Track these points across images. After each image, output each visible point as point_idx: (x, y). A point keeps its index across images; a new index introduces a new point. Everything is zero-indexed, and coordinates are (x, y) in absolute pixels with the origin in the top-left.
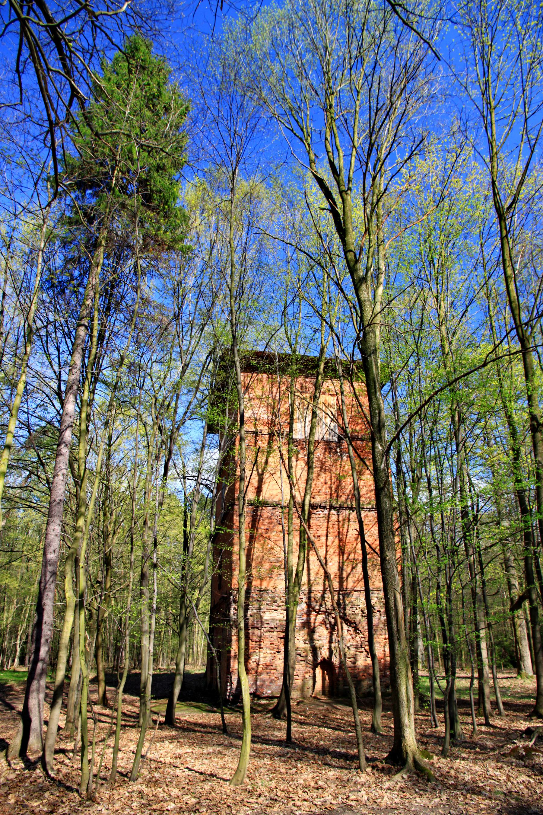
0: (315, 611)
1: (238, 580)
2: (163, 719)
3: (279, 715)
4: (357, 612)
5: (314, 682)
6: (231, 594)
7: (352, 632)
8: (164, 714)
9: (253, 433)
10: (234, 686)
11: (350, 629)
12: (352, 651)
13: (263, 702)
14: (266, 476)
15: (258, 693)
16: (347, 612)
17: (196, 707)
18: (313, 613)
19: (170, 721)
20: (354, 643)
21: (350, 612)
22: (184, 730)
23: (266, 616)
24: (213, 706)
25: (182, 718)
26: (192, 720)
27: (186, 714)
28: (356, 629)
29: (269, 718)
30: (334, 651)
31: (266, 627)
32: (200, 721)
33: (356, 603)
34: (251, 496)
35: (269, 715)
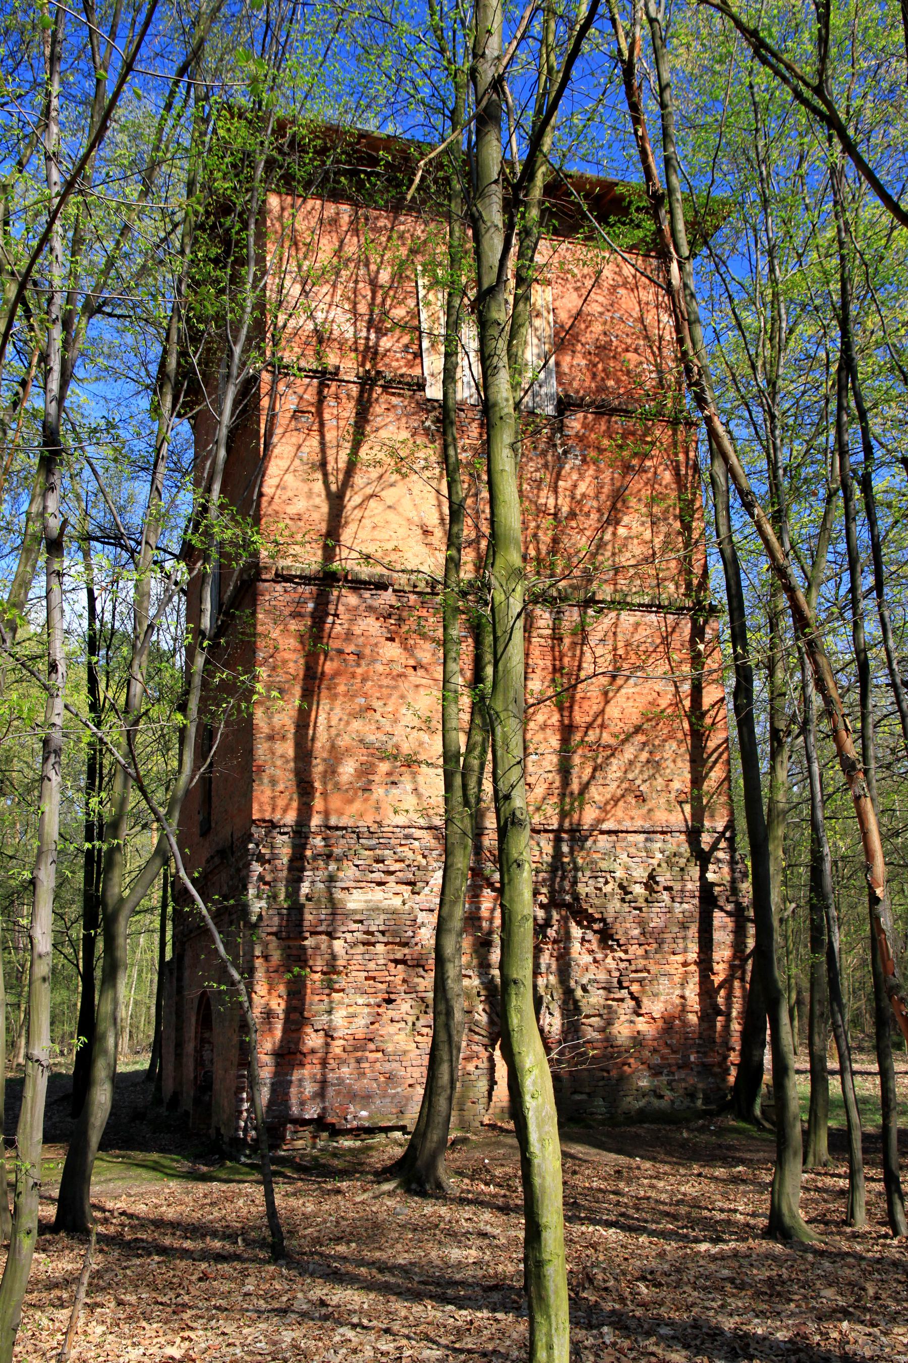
0: (491, 885)
1: (273, 799)
2: (50, 1212)
3: (421, 1184)
4: (608, 889)
5: (492, 1083)
6: (249, 837)
7: (595, 946)
8: (56, 1193)
9: (314, 374)
10: (264, 1095)
11: (590, 935)
12: (596, 998)
13: (347, 1143)
14: (352, 500)
15: (330, 1119)
16: (582, 889)
17: (155, 1167)
18: (488, 893)
19: (71, 1218)
20: (602, 976)
21: (590, 890)
22: (130, 1248)
23: (355, 901)
24: (197, 1157)
25: (110, 1205)
26: (140, 1209)
27: (126, 1190)
28: (606, 937)
29: (390, 1194)
30: (547, 998)
31: (350, 932)
32: (170, 1213)
33: (604, 865)
34: (307, 558)
35: (387, 1187)
